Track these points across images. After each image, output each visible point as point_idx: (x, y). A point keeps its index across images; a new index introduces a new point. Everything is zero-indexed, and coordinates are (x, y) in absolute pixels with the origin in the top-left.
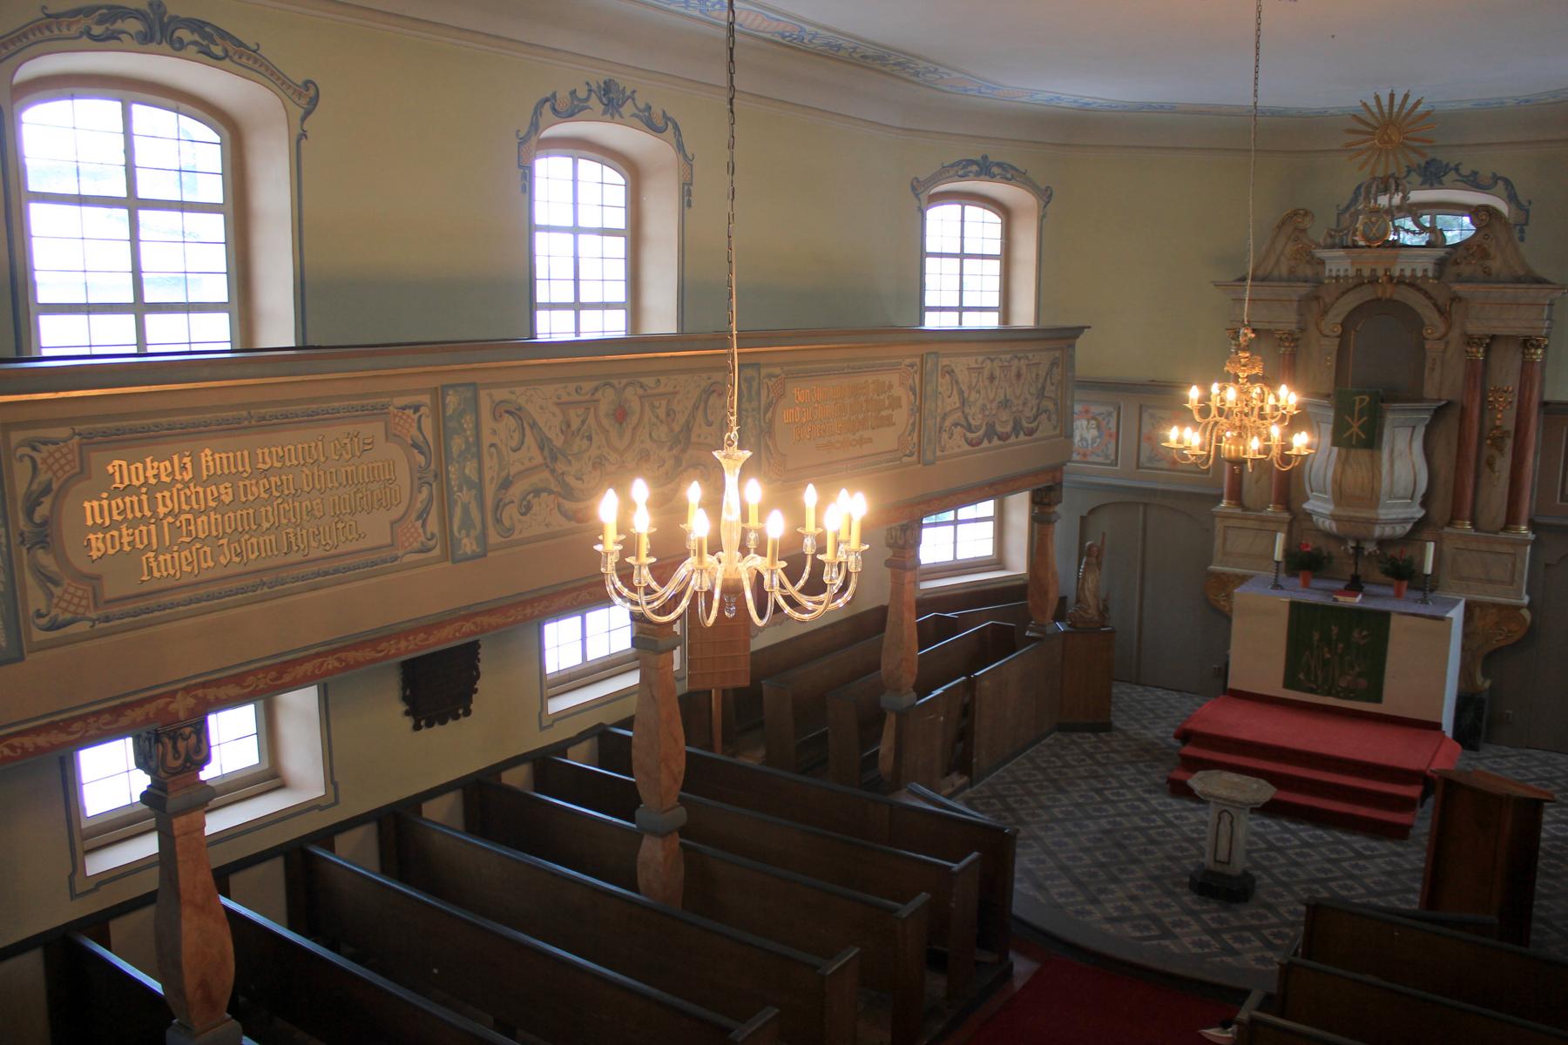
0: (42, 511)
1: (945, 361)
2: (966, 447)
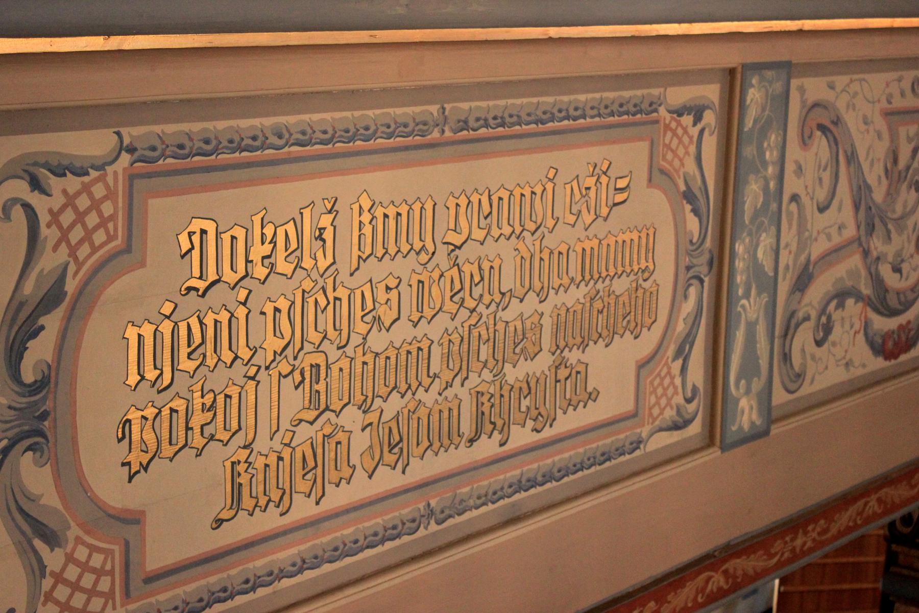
0: (40, 351)
1: (814, 88)
2: (879, 363)
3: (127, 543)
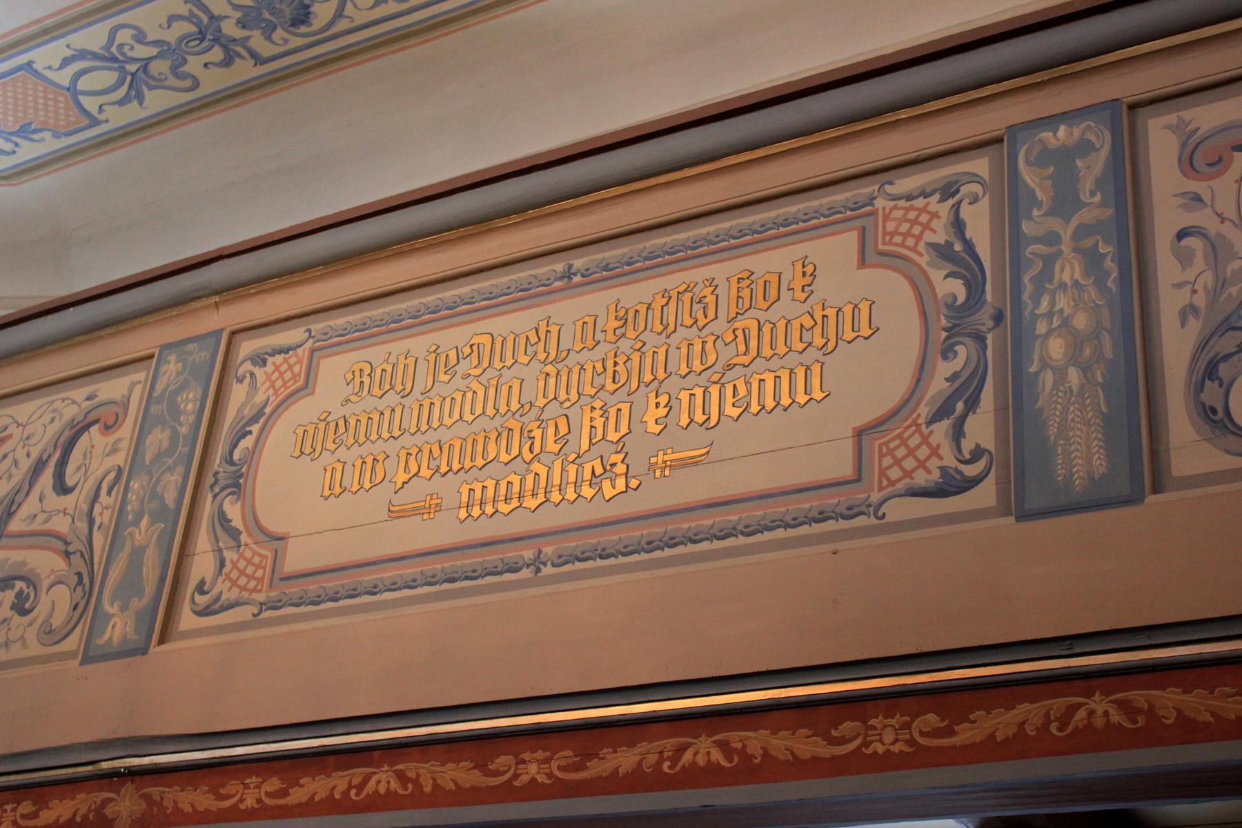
3: (276, 551)
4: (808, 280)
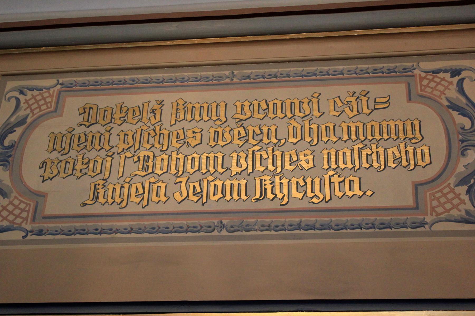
4: (123, 115)
